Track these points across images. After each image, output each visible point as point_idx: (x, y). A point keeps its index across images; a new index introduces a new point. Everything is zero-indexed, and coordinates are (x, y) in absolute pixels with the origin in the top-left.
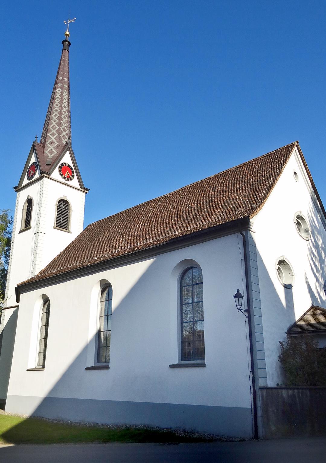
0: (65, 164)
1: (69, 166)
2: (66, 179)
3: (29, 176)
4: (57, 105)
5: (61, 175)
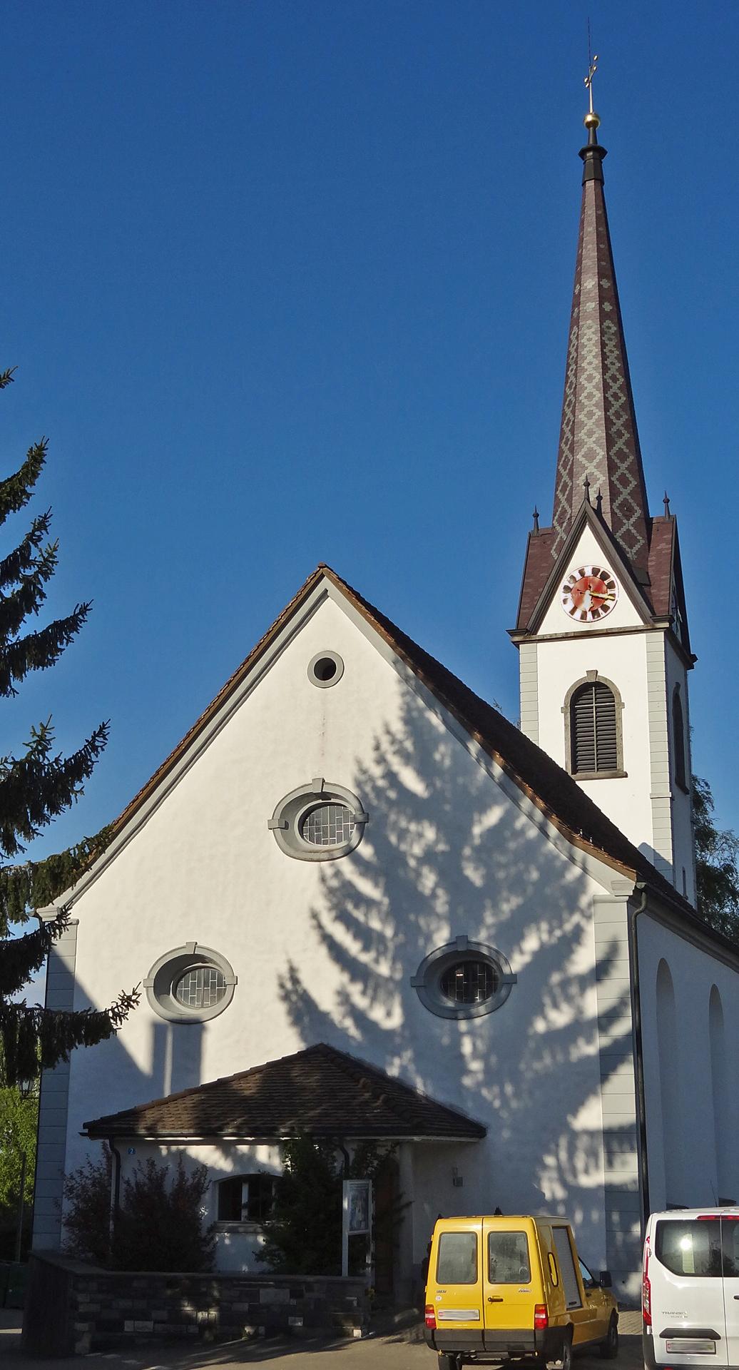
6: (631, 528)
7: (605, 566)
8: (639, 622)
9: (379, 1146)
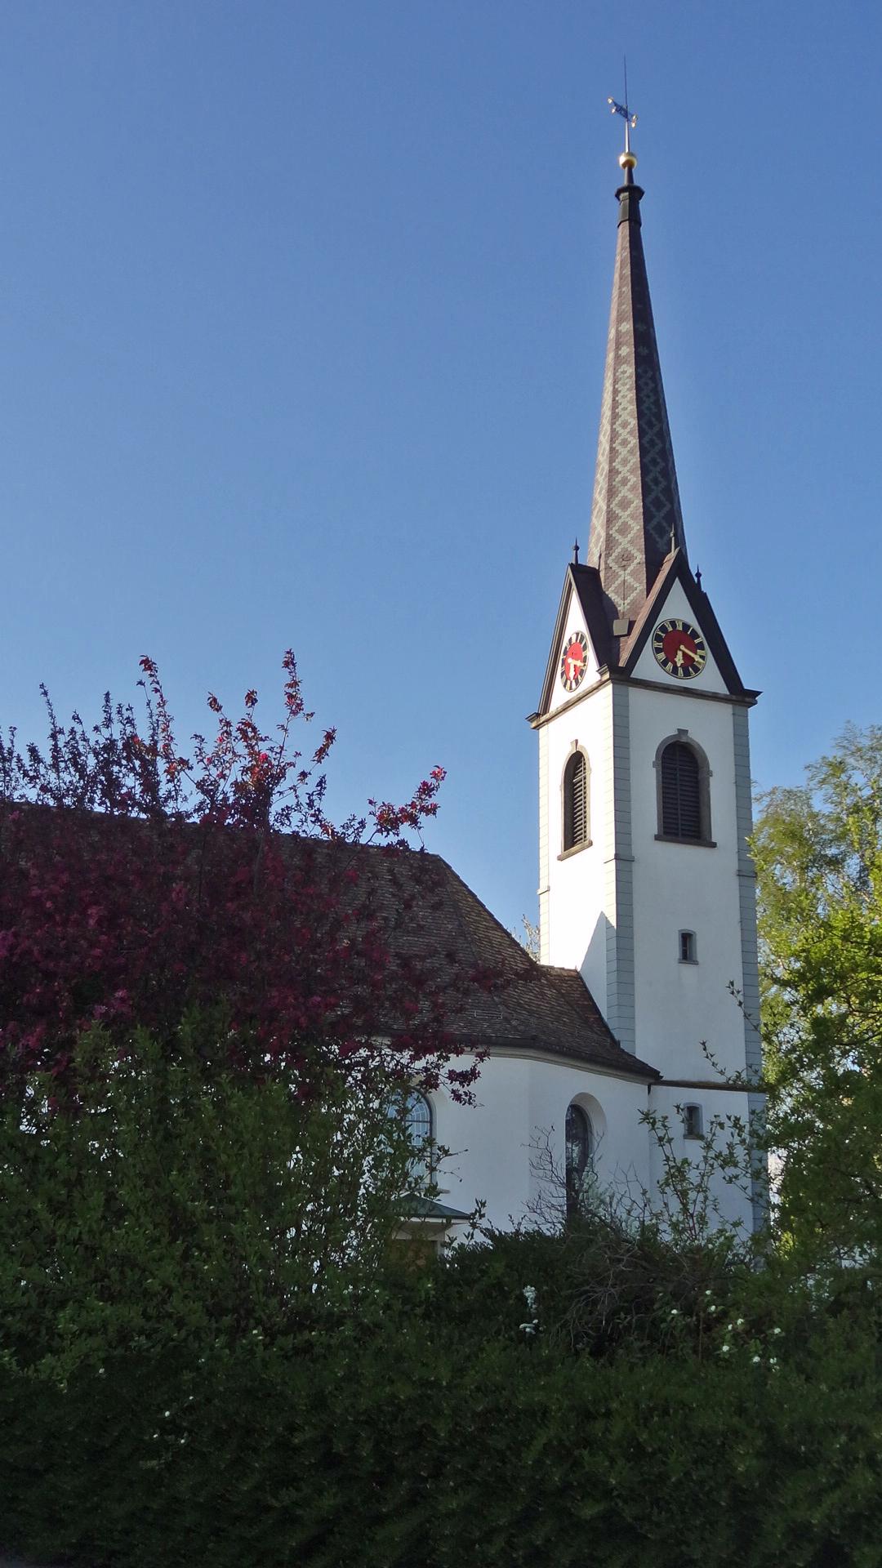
0: (673, 623)
1: (686, 626)
2: (680, 671)
3: (567, 679)
4: (625, 462)
5: (664, 664)
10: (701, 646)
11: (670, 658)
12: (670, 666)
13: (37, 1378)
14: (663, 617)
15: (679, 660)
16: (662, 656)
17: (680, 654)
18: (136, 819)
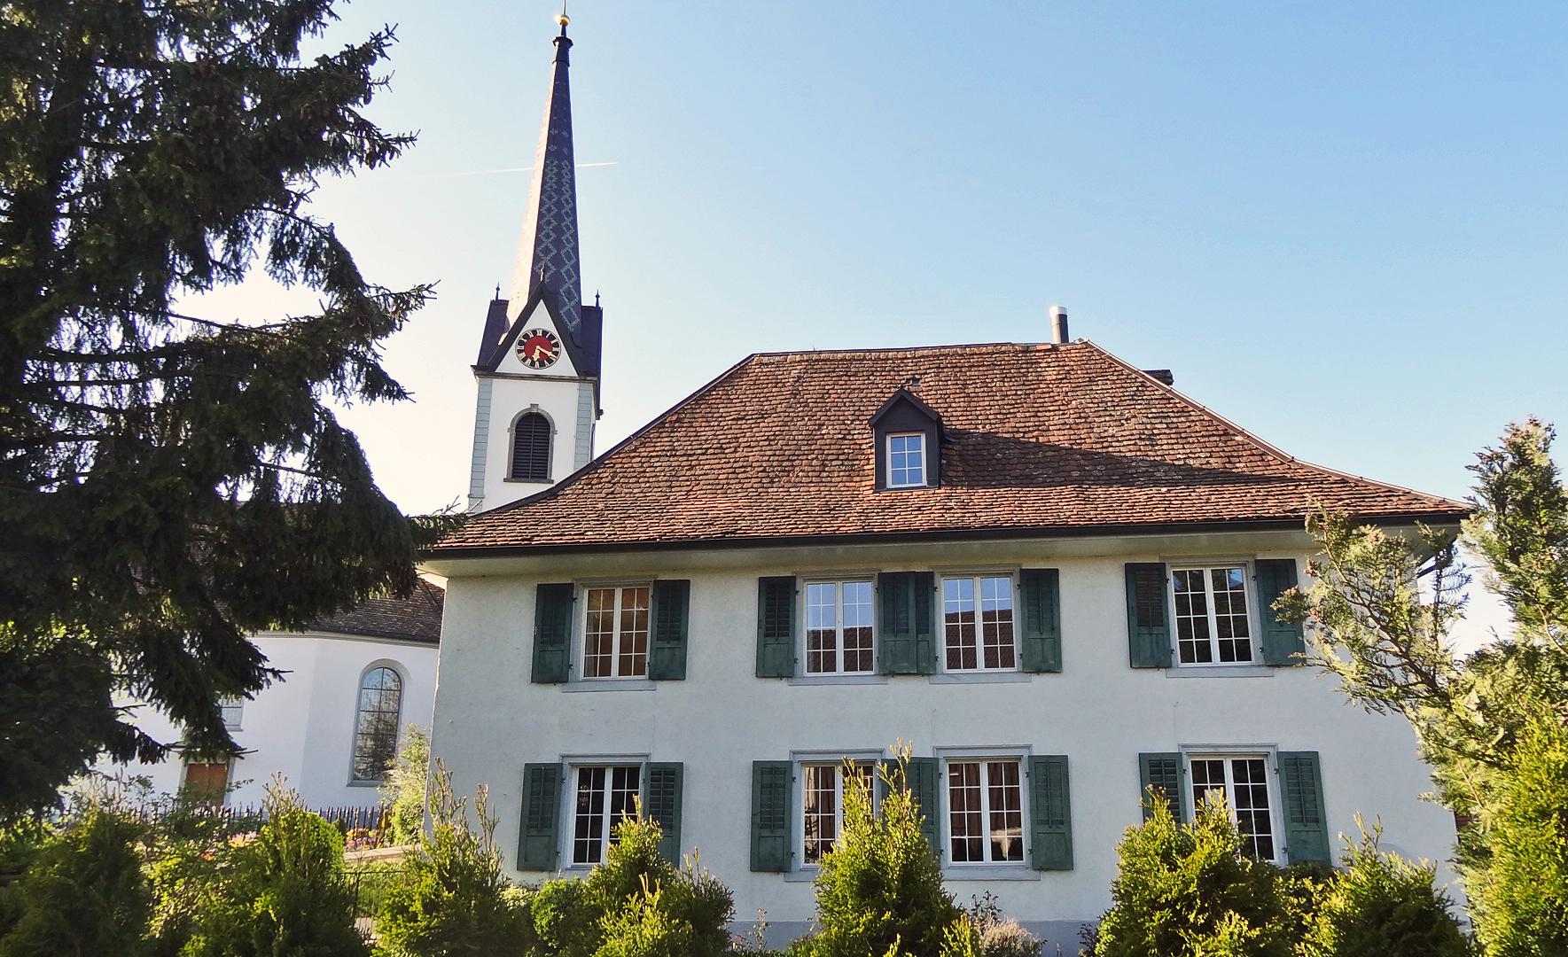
0: (534, 332)
5: (524, 360)
6: (571, 286)
7: (553, 330)
8: (575, 374)
9: (335, 167)
10: (557, 345)
11: (529, 354)
12: (529, 361)
13: (198, 936)
14: (527, 328)
15: (536, 356)
16: (523, 355)
17: (537, 352)
18: (44, 492)
